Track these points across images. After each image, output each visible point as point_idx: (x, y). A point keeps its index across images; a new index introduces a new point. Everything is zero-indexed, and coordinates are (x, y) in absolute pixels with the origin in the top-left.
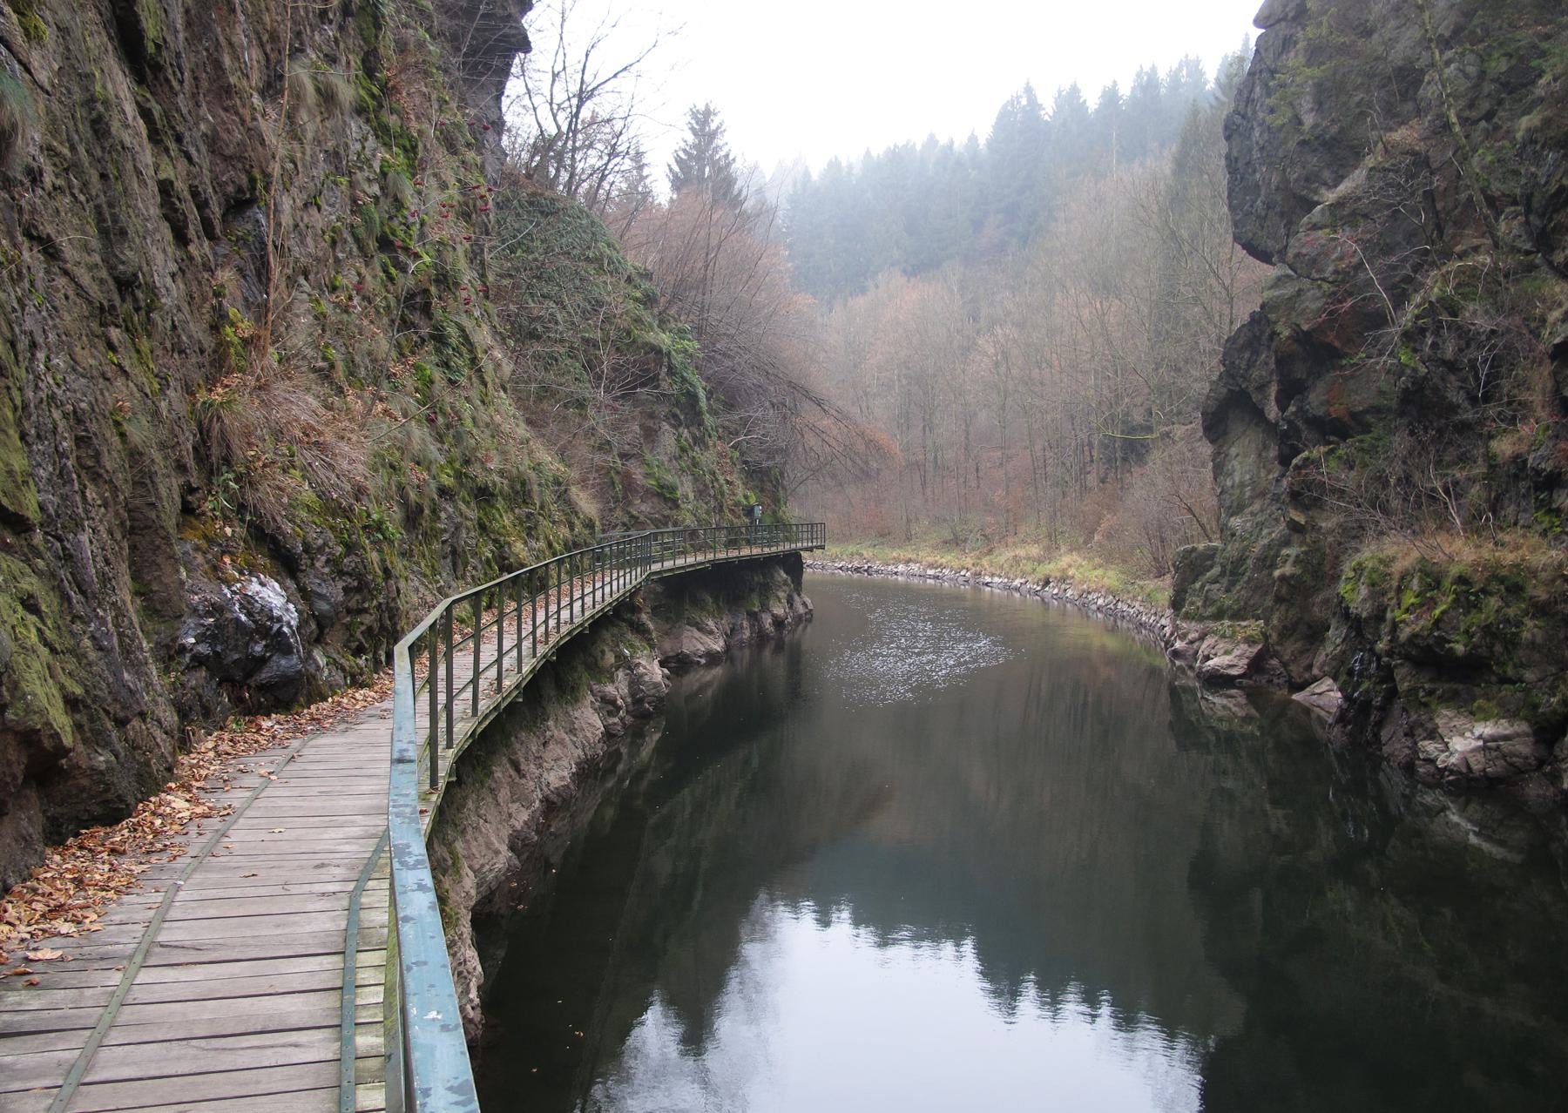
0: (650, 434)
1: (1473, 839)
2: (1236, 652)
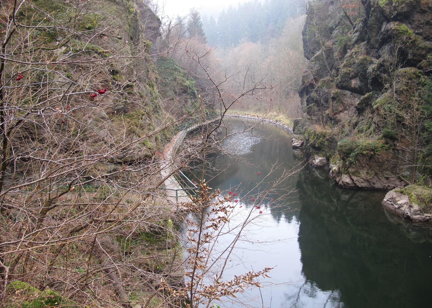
0: (186, 102)
1: (319, 176)
2: (299, 142)
